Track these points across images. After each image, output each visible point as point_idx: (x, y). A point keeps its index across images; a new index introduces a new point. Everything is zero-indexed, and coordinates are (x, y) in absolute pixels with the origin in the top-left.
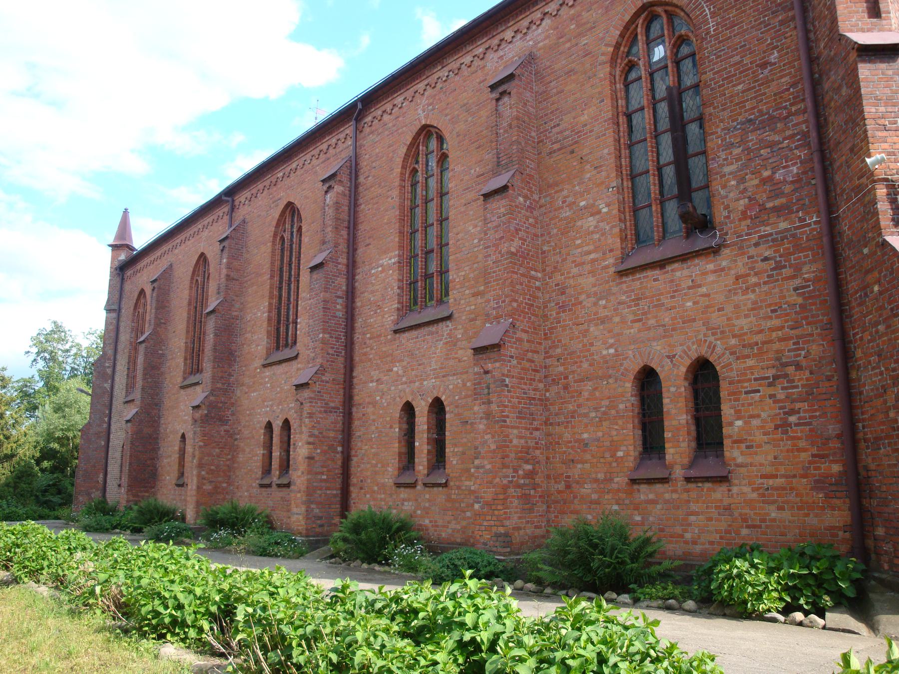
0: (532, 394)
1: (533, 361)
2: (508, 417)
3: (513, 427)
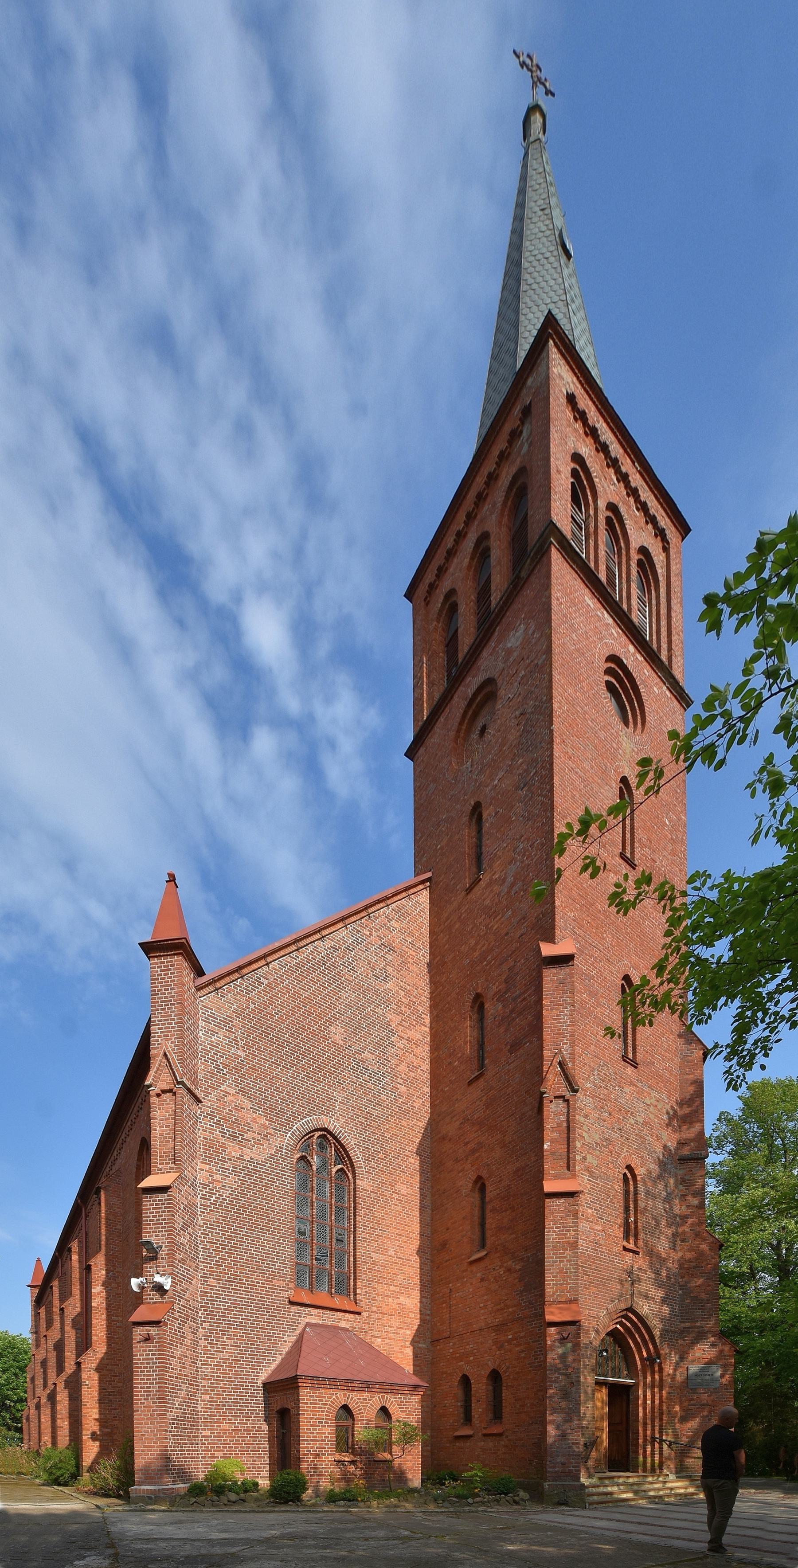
0: (111, 1389)
1: (112, 1371)
2: (88, 1402)
3: (92, 1408)
